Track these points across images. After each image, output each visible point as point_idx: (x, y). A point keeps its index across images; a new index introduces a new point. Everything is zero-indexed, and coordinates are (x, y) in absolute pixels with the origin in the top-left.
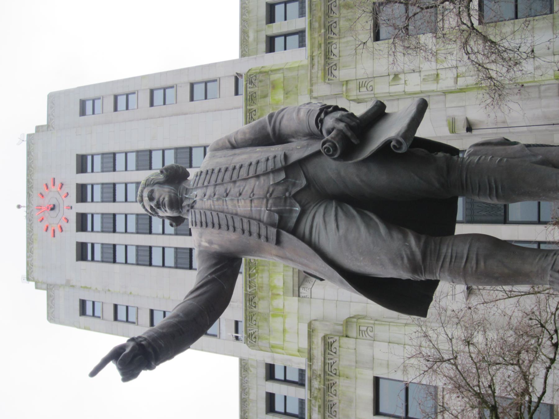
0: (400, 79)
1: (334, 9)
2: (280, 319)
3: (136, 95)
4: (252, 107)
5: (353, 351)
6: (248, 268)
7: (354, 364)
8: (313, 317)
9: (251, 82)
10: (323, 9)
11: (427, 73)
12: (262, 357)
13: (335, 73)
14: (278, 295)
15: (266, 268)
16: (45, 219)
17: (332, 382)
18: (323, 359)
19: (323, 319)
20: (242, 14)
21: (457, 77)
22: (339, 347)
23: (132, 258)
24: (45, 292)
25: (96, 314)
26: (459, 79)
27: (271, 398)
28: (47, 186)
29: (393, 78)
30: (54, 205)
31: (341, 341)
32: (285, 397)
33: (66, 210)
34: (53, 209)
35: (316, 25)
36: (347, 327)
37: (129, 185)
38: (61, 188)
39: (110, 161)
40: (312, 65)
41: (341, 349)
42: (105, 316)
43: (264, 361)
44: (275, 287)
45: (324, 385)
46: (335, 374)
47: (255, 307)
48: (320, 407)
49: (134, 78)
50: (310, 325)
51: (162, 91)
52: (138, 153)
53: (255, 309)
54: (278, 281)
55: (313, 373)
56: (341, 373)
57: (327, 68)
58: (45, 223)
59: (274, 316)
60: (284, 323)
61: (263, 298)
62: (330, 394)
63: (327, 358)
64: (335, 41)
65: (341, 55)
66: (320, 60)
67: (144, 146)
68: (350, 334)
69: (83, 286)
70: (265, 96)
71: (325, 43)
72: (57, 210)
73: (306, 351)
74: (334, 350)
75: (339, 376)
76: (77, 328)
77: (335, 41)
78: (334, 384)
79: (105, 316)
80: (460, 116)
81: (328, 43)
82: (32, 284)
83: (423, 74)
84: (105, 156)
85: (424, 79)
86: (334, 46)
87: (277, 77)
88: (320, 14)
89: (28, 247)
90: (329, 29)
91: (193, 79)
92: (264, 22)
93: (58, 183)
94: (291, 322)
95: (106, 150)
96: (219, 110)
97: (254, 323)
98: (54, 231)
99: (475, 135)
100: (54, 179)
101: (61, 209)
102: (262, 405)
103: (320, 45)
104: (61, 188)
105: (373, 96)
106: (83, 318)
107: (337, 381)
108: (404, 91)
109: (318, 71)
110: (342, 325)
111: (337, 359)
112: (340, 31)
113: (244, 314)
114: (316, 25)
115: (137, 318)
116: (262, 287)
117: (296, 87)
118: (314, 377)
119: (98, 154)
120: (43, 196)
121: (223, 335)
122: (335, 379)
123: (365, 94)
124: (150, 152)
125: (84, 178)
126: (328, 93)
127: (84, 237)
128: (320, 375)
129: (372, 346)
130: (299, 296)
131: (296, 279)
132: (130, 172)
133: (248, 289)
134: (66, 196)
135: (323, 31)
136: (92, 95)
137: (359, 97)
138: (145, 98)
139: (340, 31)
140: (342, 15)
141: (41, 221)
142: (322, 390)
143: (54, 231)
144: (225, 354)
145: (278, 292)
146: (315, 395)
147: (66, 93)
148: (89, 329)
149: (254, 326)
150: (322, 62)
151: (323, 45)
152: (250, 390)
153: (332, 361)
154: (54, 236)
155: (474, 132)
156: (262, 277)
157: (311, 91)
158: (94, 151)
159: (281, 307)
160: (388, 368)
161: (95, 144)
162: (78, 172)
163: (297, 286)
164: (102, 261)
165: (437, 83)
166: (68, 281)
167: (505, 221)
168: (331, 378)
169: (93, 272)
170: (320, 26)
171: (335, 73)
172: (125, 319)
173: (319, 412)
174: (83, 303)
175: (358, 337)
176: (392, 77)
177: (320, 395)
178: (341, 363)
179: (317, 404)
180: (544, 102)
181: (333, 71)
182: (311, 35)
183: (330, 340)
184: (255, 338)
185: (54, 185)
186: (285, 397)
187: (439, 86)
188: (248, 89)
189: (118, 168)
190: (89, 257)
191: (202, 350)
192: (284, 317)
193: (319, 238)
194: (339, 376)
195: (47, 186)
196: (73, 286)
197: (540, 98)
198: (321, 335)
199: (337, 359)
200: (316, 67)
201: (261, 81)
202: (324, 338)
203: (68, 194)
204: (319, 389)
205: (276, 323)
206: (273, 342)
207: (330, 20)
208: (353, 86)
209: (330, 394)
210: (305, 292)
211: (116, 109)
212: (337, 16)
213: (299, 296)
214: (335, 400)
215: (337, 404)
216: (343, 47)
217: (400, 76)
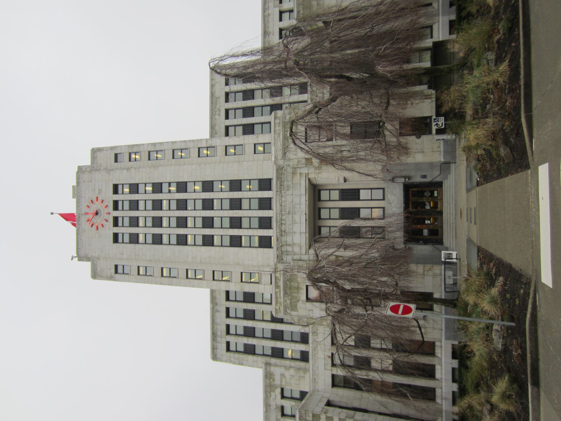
12: (223, 287)
33: (106, 215)
34: (97, 213)
42: (155, 275)
72: (99, 214)
95: (133, 182)
102: (224, 314)
106: (117, 275)
127: (116, 230)
132: (189, 229)
167: (358, 199)
169: (126, 250)
174: (116, 267)
185: (97, 200)
193: (244, 55)
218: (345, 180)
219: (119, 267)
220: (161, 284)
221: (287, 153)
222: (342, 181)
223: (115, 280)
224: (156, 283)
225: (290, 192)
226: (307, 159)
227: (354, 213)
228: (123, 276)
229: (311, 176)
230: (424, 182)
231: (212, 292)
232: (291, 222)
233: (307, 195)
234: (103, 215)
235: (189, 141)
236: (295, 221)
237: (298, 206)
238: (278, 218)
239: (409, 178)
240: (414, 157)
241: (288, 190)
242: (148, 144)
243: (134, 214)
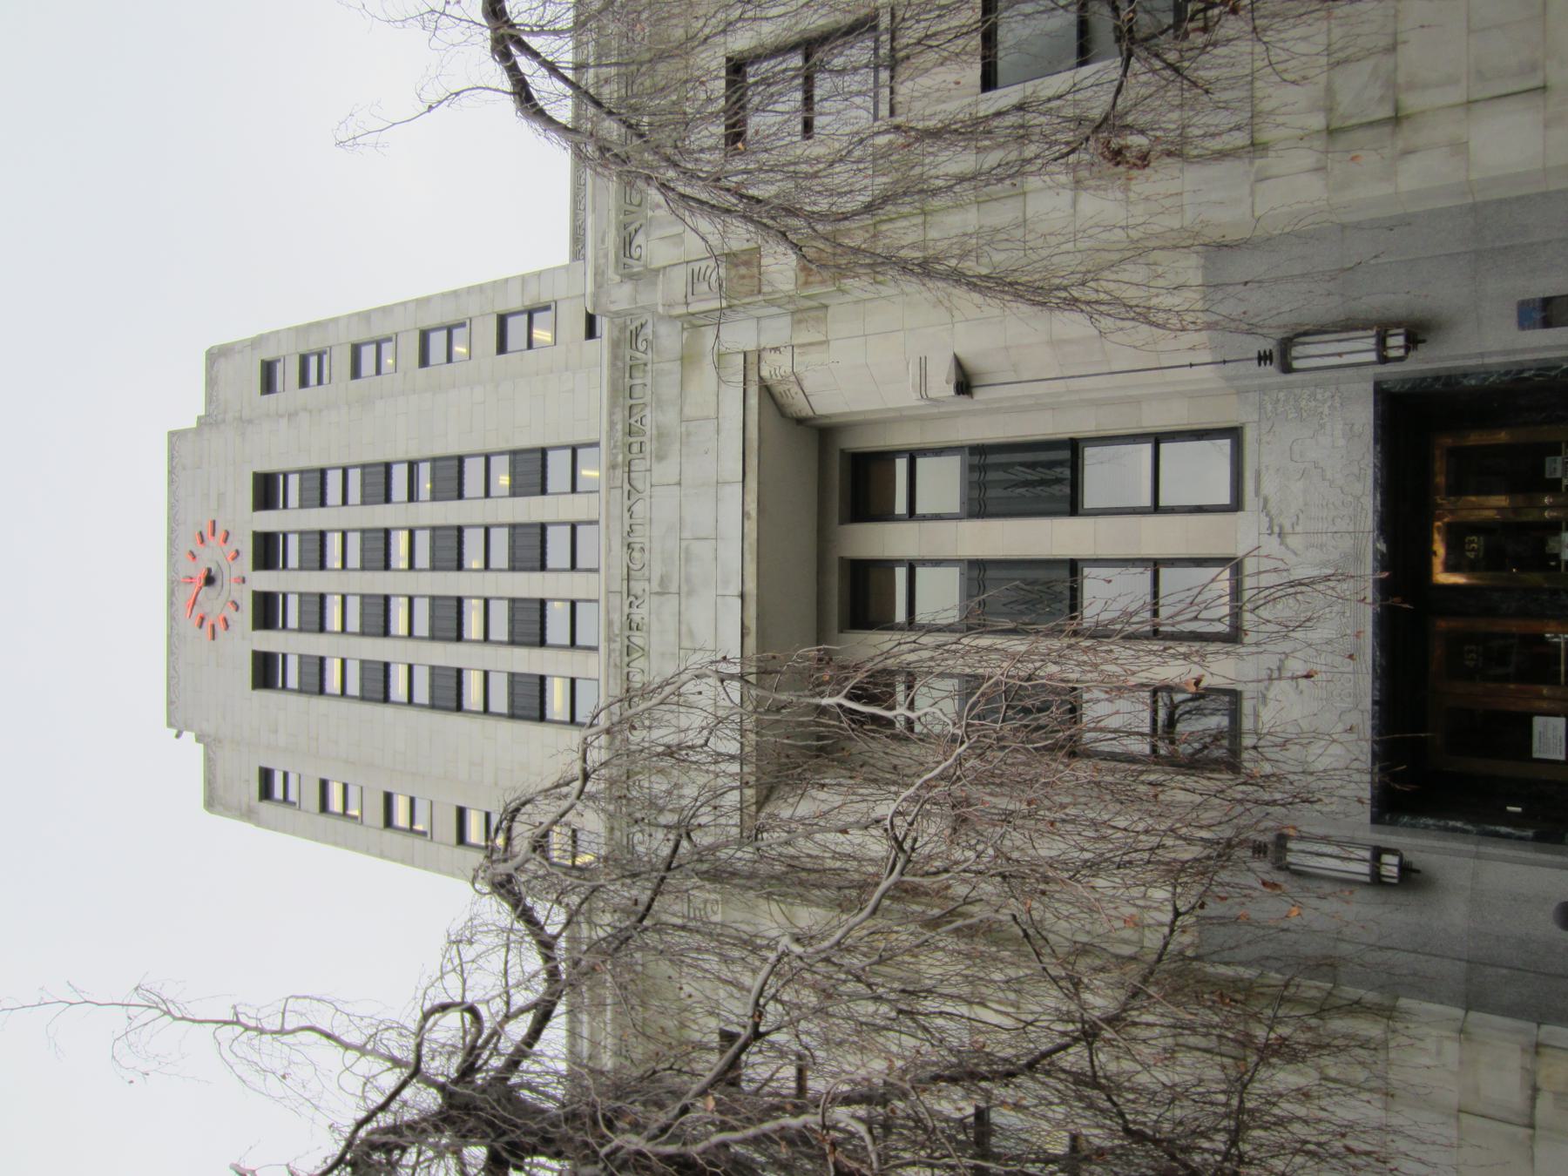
23: (500, 702)
33: (235, 586)
34: (210, 580)
37: (493, 531)
39: (316, 488)
51: (445, 332)
72: (219, 582)
98: (213, 627)
104: (225, 540)
106: (265, 805)
119: (501, 453)
124: (544, 452)
125: (269, 521)
127: (269, 641)
143: (213, 627)
161: (283, 452)
174: (266, 776)
189: (467, 492)
203: (237, 552)
218: (965, 384)
220: (382, 855)
221: (639, 239)
222: (942, 384)
223: (259, 824)
224: (368, 851)
225: (666, 471)
226: (732, 258)
227: (1050, 592)
229: (775, 367)
230: (1544, 368)
232: (673, 638)
233: (752, 484)
234: (226, 587)
235: (469, 290)
236: (691, 633)
237: (702, 550)
238: (616, 617)
239: (1416, 335)
240: (1459, 148)
241: (660, 457)
242: (350, 316)
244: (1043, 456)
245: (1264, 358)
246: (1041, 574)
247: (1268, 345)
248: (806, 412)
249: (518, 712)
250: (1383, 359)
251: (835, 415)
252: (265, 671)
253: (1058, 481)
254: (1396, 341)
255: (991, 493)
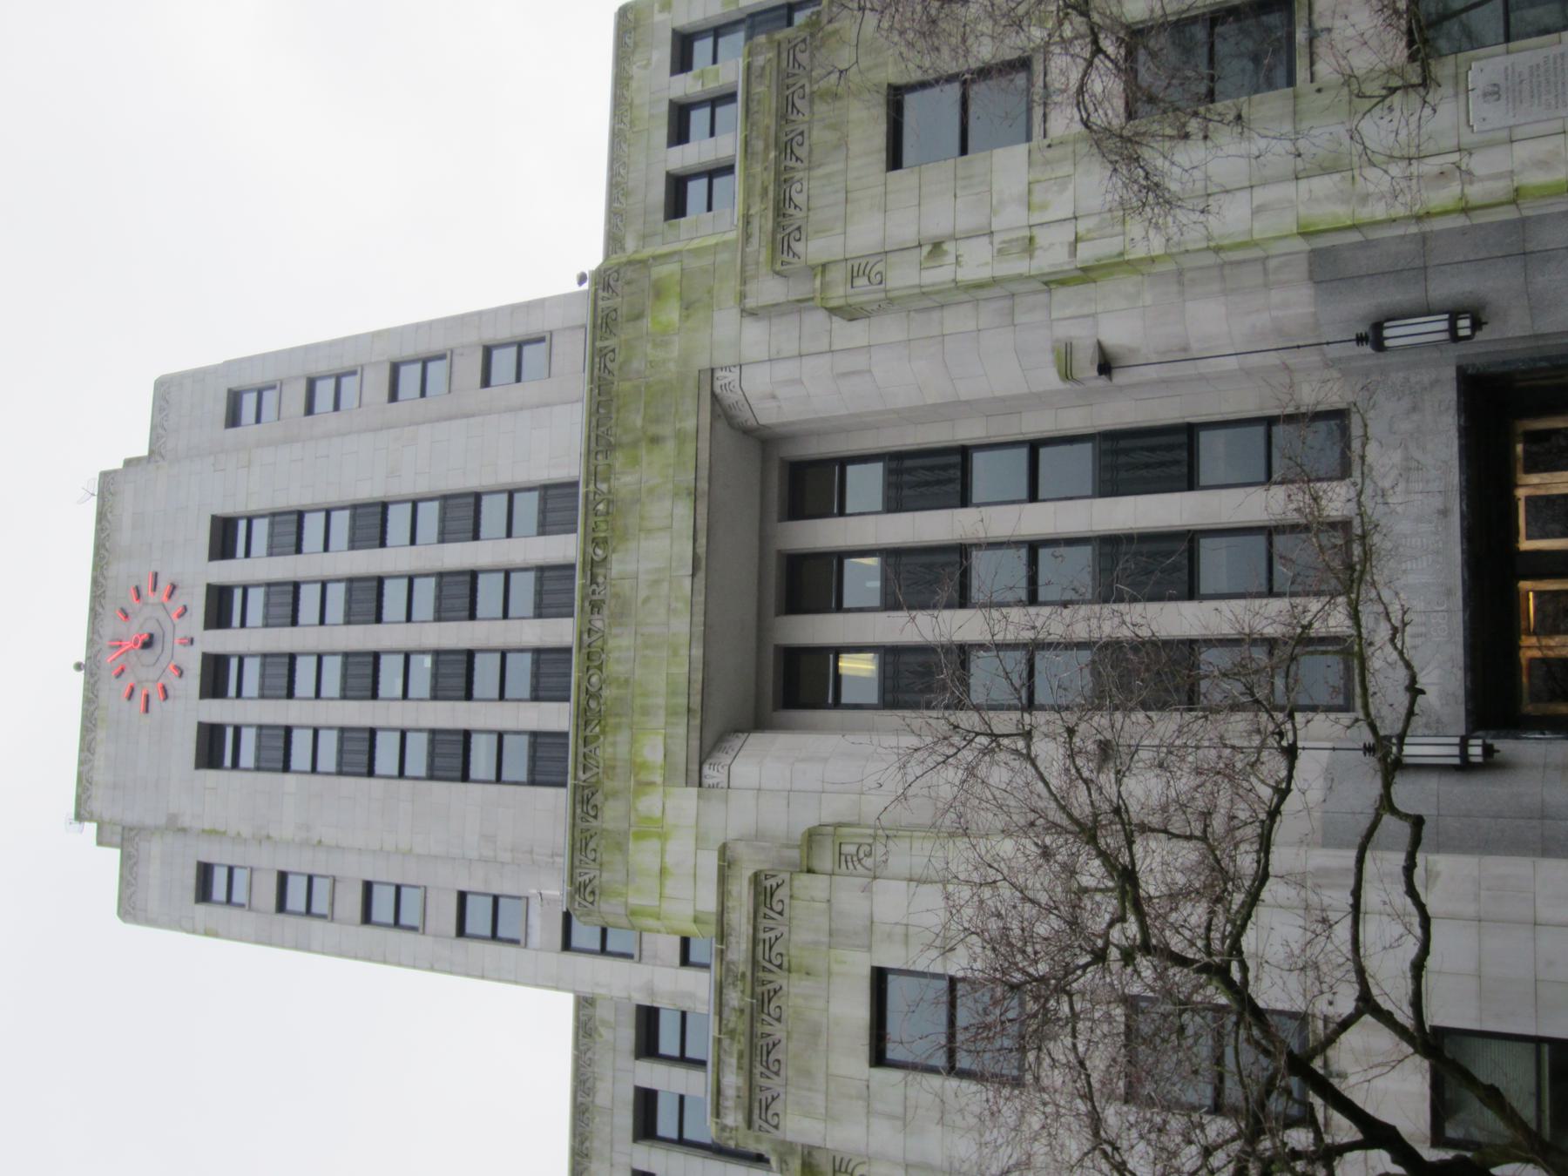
0: (945, 253)
1: (798, 103)
2: (654, 844)
3: (358, 377)
4: (606, 343)
5: (825, 905)
6: (582, 723)
7: (825, 939)
8: (731, 835)
9: (607, 287)
10: (774, 105)
11: (1007, 237)
13: (798, 247)
14: (652, 784)
15: (624, 720)
16: (128, 670)
17: (770, 986)
18: (751, 931)
19: (757, 837)
20: (612, 198)
21: (1077, 240)
22: (791, 897)
24: (117, 853)
25: (236, 898)
26: (1079, 245)
27: (646, 1101)
28: (138, 590)
29: (930, 252)
30: (151, 636)
31: (796, 883)
32: (682, 1098)
34: (148, 644)
35: (759, 145)
36: (810, 848)
38: (170, 595)
39: (290, 528)
40: (747, 237)
41: (795, 902)
43: (629, 999)
44: (644, 766)
45: (752, 997)
46: (780, 967)
47: (595, 817)
48: (741, 1056)
49: (357, 338)
50: (723, 850)
52: (356, 508)
53: (594, 823)
54: (652, 750)
55: (728, 970)
56: (793, 961)
57: (779, 237)
58: (128, 679)
59: (641, 836)
60: (663, 852)
61: (615, 794)
62: (765, 1017)
63: (761, 927)
64: (798, 175)
65: (812, 205)
66: (764, 223)
67: (368, 491)
68: (816, 865)
69: (207, 827)
70: (639, 316)
71: (777, 179)
72: (157, 648)
73: (713, 919)
74: (778, 907)
75: (789, 971)
76: (188, 932)
77: (798, 175)
78: (775, 992)
79: (255, 902)
80: (1083, 336)
81: (783, 180)
82: (91, 828)
83: (997, 239)
84: (278, 519)
85: (1000, 251)
86: (797, 186)
87: (668, 270)
88: (767, 121)
89: (83, 738)
90: (786, 148)
91: (489, 336)
92: (661, 216)
93: (163, 585)
94: (680, 848)
96: (547, 405)
97: (591, 856)
98: (147, 697)
99: (1121, 388)
100: (156, 575)
101: (168, 646)
102: (625, 1119)
103: (765, 190)
104: (170, 595)
105: (883, 295)
106: (202, 908)
107: (784, 983)
108: (955, 281)
109: (759, 249)
110: (799, 847)
111: (785, 929)
112: (810, 152)
113: (568, 837)
114: (759, 145)
115: (332, 904)
116: (614, 768)
117: (710, 291)
118: (730, 980)
120: (126, 617)
121: (536, 937)
122: (779, 979)
123: (866, 293)
125: (228, 572)
126: (782, 299)
128: (743, 975)
129: (866, 889)
130: (700, 785)
131: (695, 743)
133: (580, 773)
134: (180, 615)
135: (772, 155)
136: (258, 379)
137: (851, 301)
138: (378, 382)
139: (810, 152)
140: (817, 117)
141: (118, 675)
142: (748, 1011)
143: (147, 697)
144: (537, 986)
145: (651, 778)
146: (731, 1025)
147: (198, 377)
148: (216, 935)
149: (592, 865)
150: (769, 225)
151: (771, 188)
152: (598, 1084)
153: (772, 935)
154: (147, 710)
155: (1120, 377)
156: (614, 744)
157: (743, 296)
158: (253, 507)
159: (658, 814)
160: (907, 943)
162: (214, 556)
163: (696, 760)
164: (258, 769)
165: (1031, 257)
166: (172, 818)
168: (769, 977)
169: (233, 795)
170: (767, 148)
171: (798, 247)
172: (303, 908)
173: (740, 1067)
174: (205, 872)
175: (837, 870)
176: (926, 249)
177: (742, 1026)
178: (794, 937)
179: (736, 1048)
180: (1276, 296)
181: (793, 244)
182: (746, 168)
183: (768, 883)
184: (593, 893)
186: (682, 1098)
187: (1035, 263)
188: (600, 303)
190: (228, 761)
191: (483, 977)
192: (663, 837)
194: (789, 971)
195: (138, 590)
196: (184, 830)
197: (1267, 286)
198: (748, 873)
199: (785, 929)
200: (755, 241)
201: (628, 283)
202: (756, 879)
203: (185, 609)
204: (742, 1011)
205: (644, 855)
206: (635, 901)
207: (788, 129)
208: (837, 274)
209: (765, 1017)
210: (715, 773)
211: (310, 410)
212: (806, 118)
213: (700, 785)
214: (778, 1031)
215: (784, 1042)
216: (816, 189)
217: (946, 247)
219: (291, 880)
228: (395, 935)
231: (584, 1004)
243: (304, 654)
244: (1164, 440)
245: (1360, 339)
246: (925, 559)
247: (1363, 329)
248: (751, 422)
249: (263, 765)
250: (1455, 338)
251: (793, 423)
252: (212, 747)
253: (1177, 462)
254: (1464, 323)
255: (906, 492)
